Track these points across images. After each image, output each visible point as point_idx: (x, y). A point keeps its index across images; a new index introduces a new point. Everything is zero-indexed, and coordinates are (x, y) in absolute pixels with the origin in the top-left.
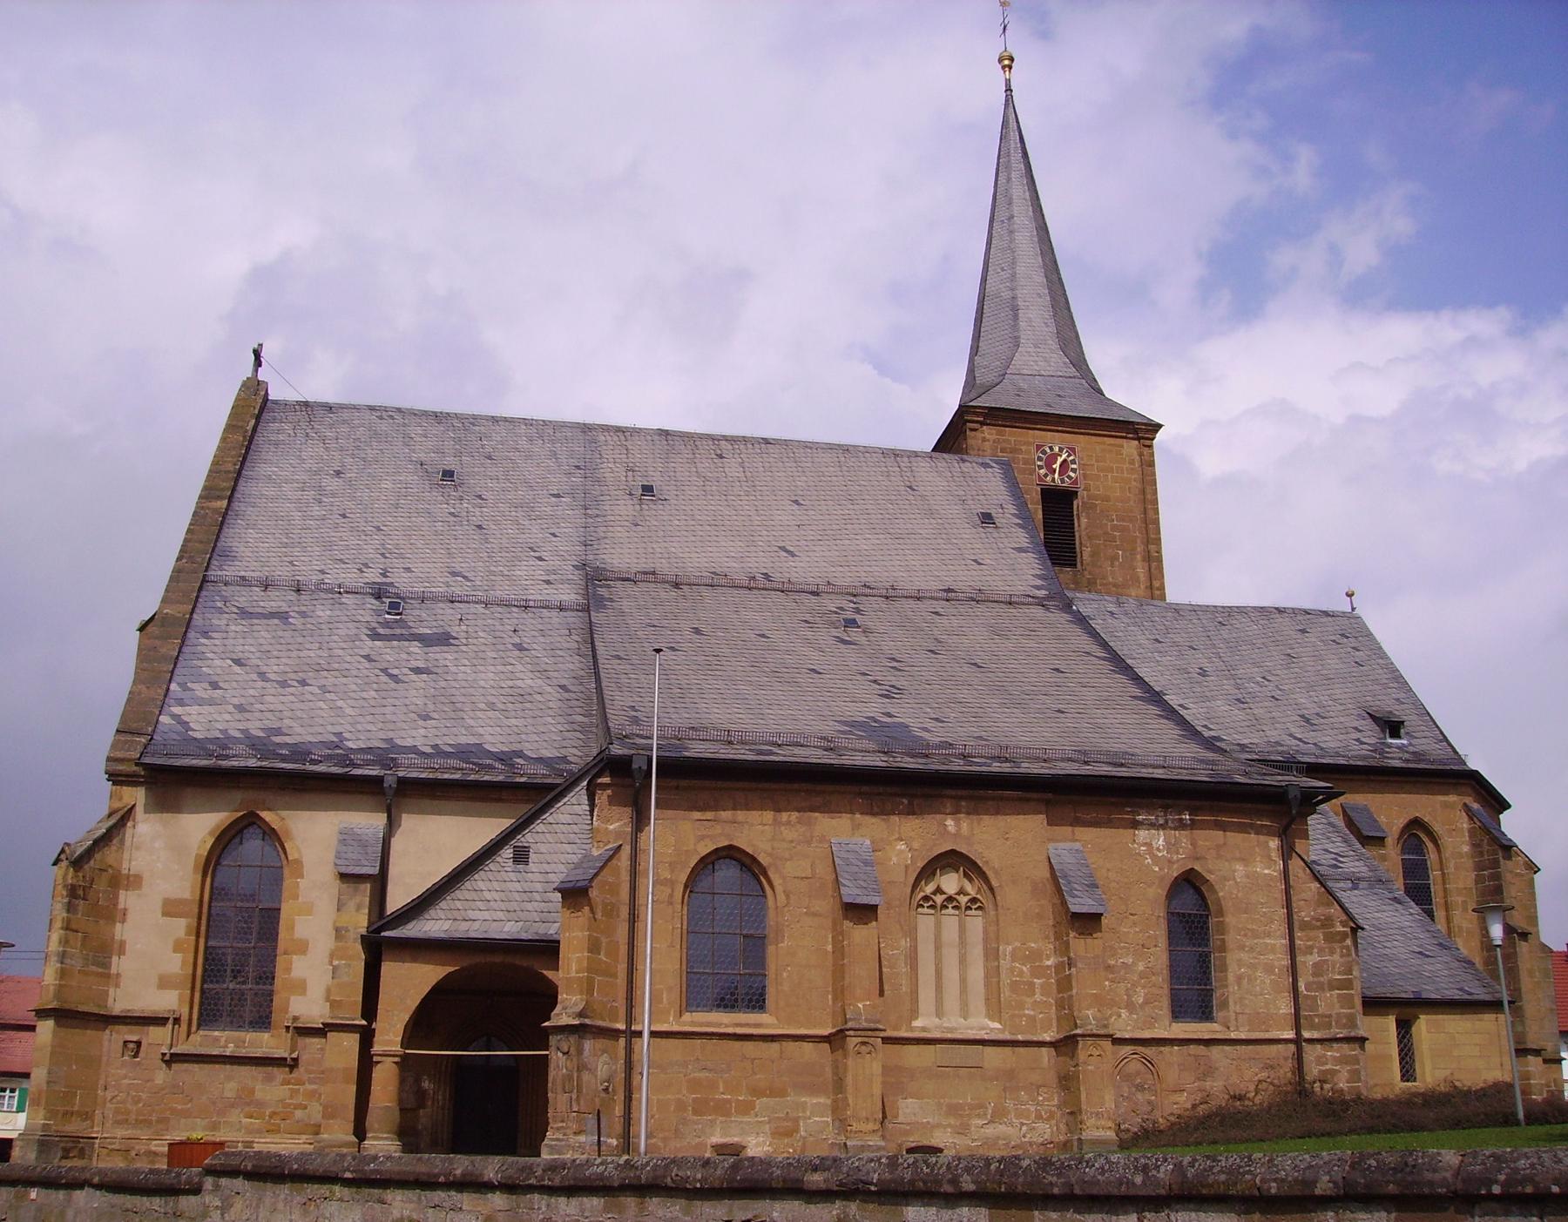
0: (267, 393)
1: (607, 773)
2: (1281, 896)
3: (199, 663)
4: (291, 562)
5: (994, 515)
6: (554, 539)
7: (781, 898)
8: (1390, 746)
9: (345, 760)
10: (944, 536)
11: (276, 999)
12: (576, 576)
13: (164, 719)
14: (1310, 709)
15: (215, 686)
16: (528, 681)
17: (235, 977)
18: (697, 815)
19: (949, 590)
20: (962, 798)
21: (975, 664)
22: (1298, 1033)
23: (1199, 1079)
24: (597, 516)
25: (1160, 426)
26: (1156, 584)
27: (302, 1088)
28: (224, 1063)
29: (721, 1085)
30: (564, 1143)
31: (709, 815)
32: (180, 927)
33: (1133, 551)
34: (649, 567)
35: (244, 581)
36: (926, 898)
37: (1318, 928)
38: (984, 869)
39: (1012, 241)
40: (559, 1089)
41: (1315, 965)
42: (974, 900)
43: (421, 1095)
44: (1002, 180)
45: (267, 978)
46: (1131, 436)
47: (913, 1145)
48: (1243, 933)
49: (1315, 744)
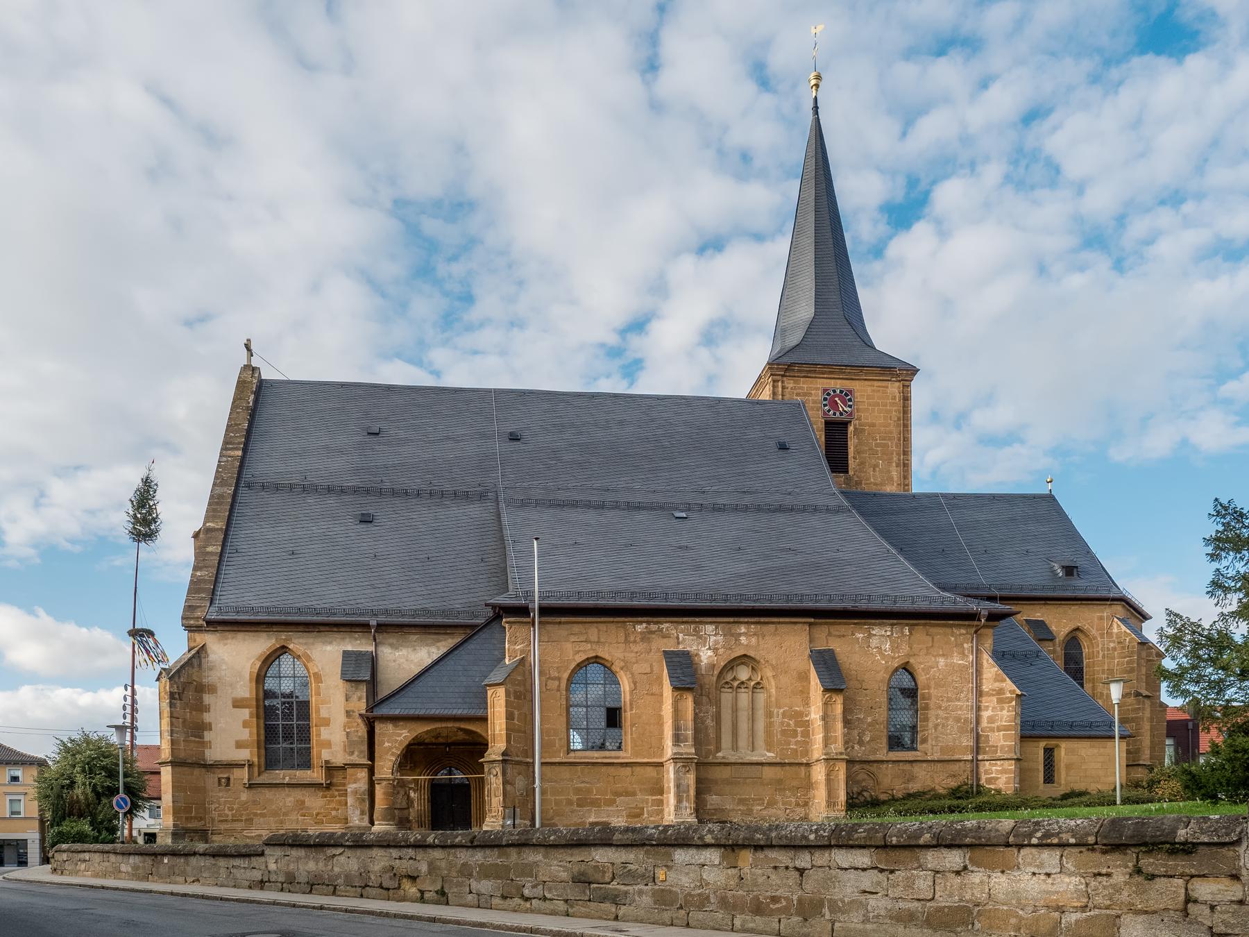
30: (496, 824)
32: (245, 713)
37: (993, 695)
45: (306, 740)
48: (941, 699)
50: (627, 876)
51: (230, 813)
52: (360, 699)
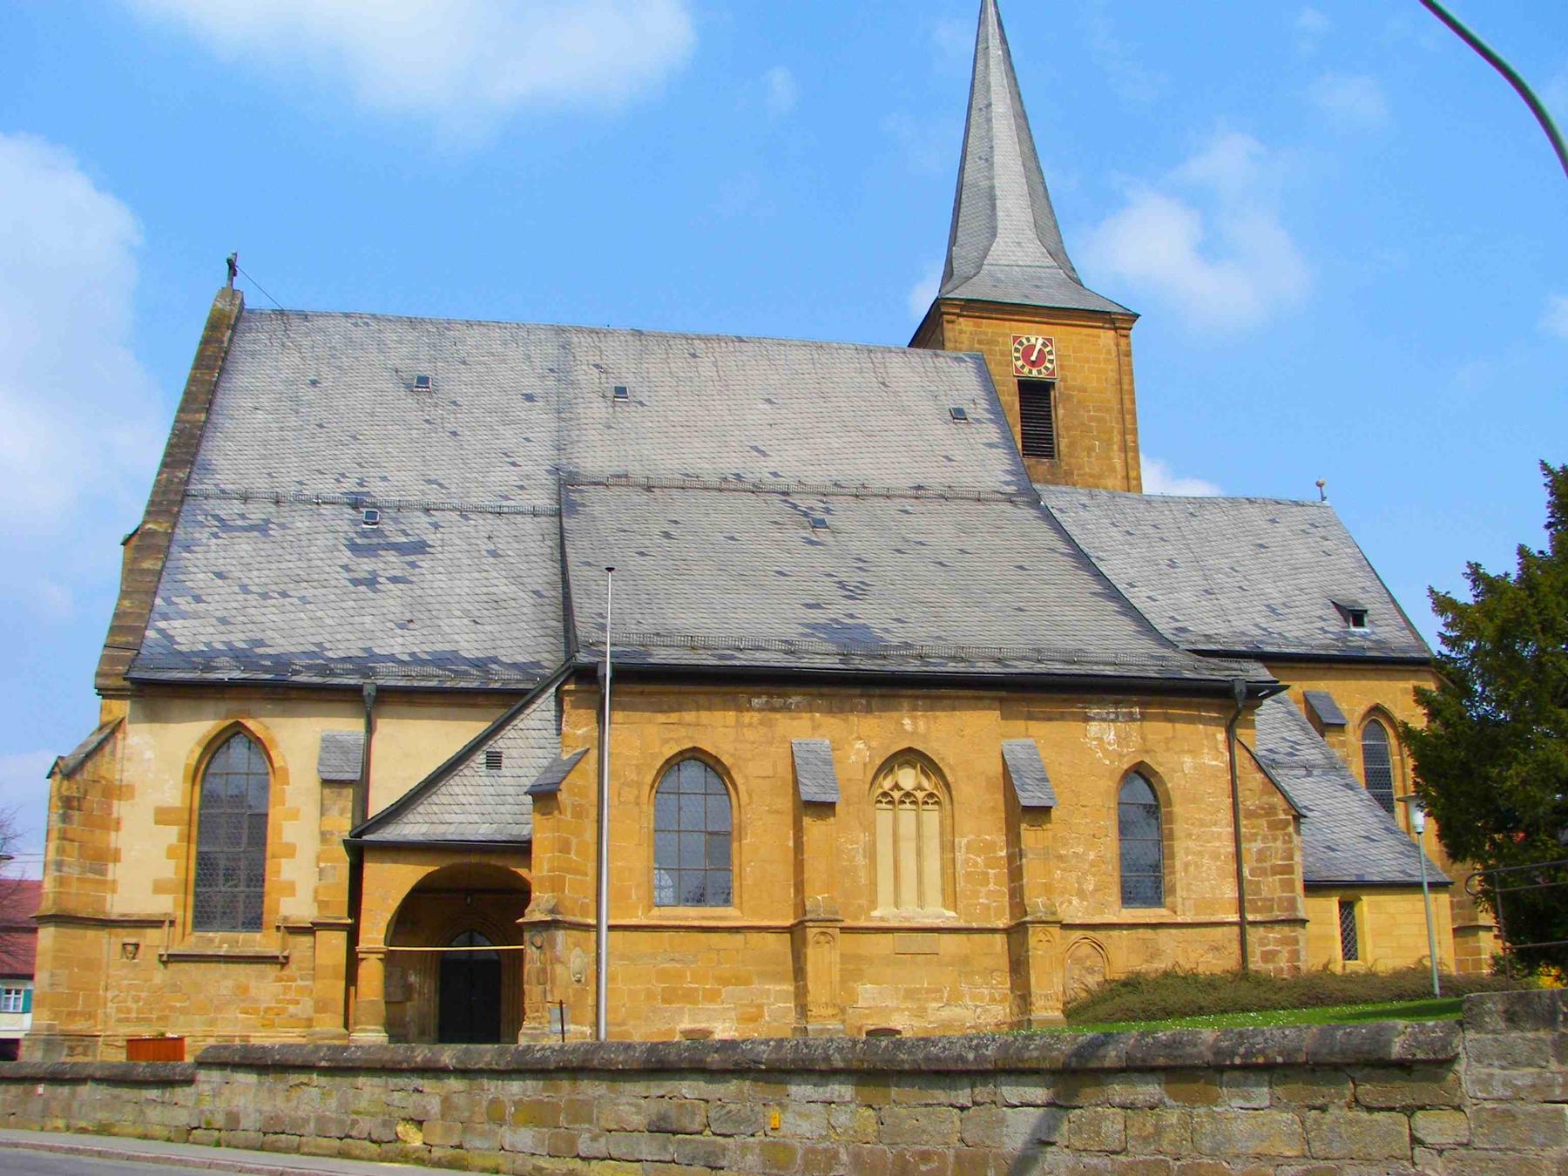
0: (242, 303)
1: (573, 679)
2: (1227, 788)
3: (181, 577)
4: (269, 474)
5: (966, 410)
6: (528, 444)
7: (744, 797)
8: (1352, 634)
9: (324, 670)
10: (915, 433)
11: (266, 900)
12: (549, 481)
13: (151, 634)
14: (1277, 600)
15: (198, 599)
16: (504, 588)
17: (227, 880)
18: (661, 718)
19: (919, 488)
20: (917, 697)
21: (940, 563)
22: (1242, 916)
23: (1147, 961)
24: (571, 419)
25: (1139, 316)
26: (1133, 474)
27: (294, 984)
28: (219, 962)
29: (688, 974)
30: (539, 1031)
31: (674, 717)
32: (172, 834)
33: (1109, 442)
34: (620, 471)
35: (224, 495)
36: (885, 794)
37: (1261, 816)
38: (940, 765)
39: (990, 129)
40: (534, 981)
41: (1260, 852)
42: (931, 795)
43: (408, 990)
44: (980, 66)
45: (258, 881)
46: (1107, 326)
47: (873, 1027)
48: (1190, 822)
49: (1280, 634)
50: (726, 1121)
51: (134, 1006)
52: (342, 813)
